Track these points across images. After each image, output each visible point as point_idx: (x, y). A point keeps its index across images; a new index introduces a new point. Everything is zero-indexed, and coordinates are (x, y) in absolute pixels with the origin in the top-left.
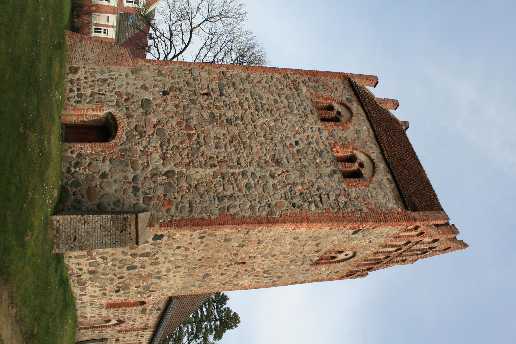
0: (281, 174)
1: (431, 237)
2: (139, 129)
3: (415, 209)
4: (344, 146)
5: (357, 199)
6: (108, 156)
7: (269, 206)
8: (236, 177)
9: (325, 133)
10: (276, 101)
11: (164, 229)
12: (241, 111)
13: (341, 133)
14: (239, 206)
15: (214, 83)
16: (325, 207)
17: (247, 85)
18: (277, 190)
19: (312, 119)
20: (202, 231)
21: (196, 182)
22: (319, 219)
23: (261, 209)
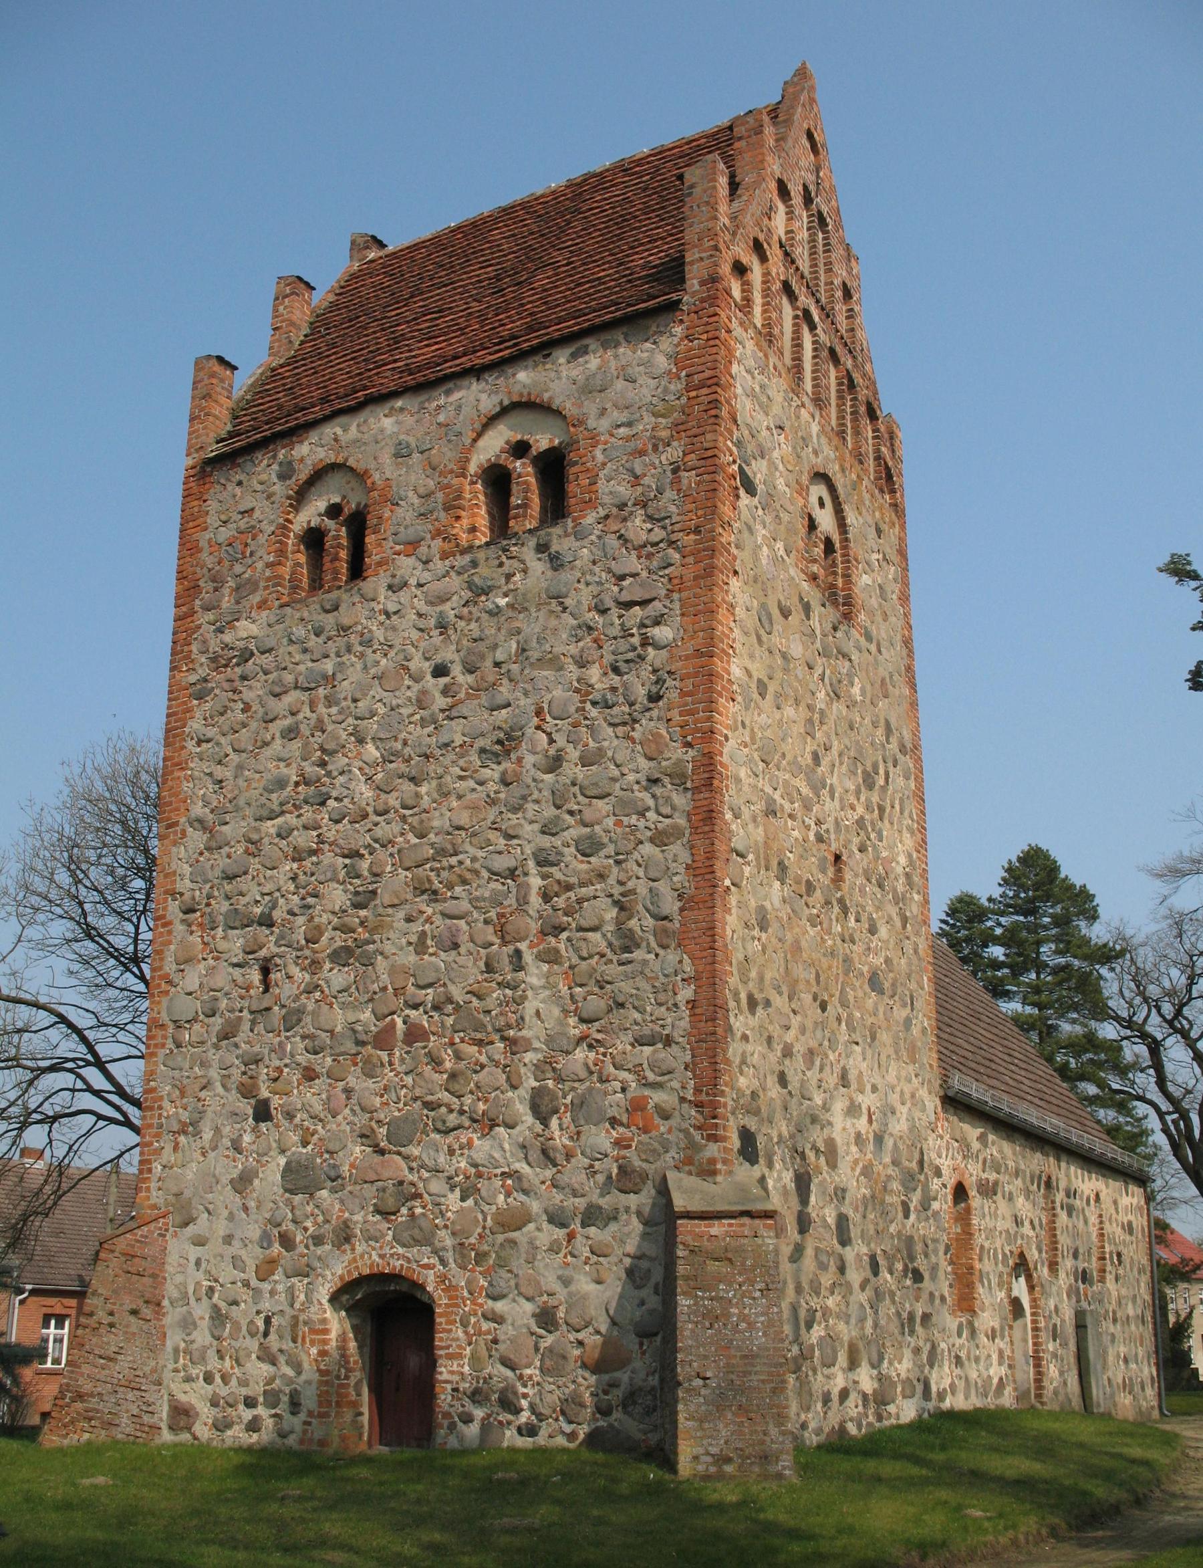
0: (549, 734)
1: (769, 213)
2: (391, 1203)
3: (673, 272)
4: (453, 506)
5: (636, 477)
6: (481, 1305)
7: (656, 781)
8: (556, 888)
9: (407, 566)
10: (291, 734)
11: (725, 1127)
12: (328, 858)
13: (405, 513)
14: (654, 881)
15: (222, 945)
16: (663, 592)
17: (233, 830)
18: (601, 752)
19: (354, 612)
20: (732, 1004)
21: (572, 1021)
22: (704, 615)
23: (666, 810)
